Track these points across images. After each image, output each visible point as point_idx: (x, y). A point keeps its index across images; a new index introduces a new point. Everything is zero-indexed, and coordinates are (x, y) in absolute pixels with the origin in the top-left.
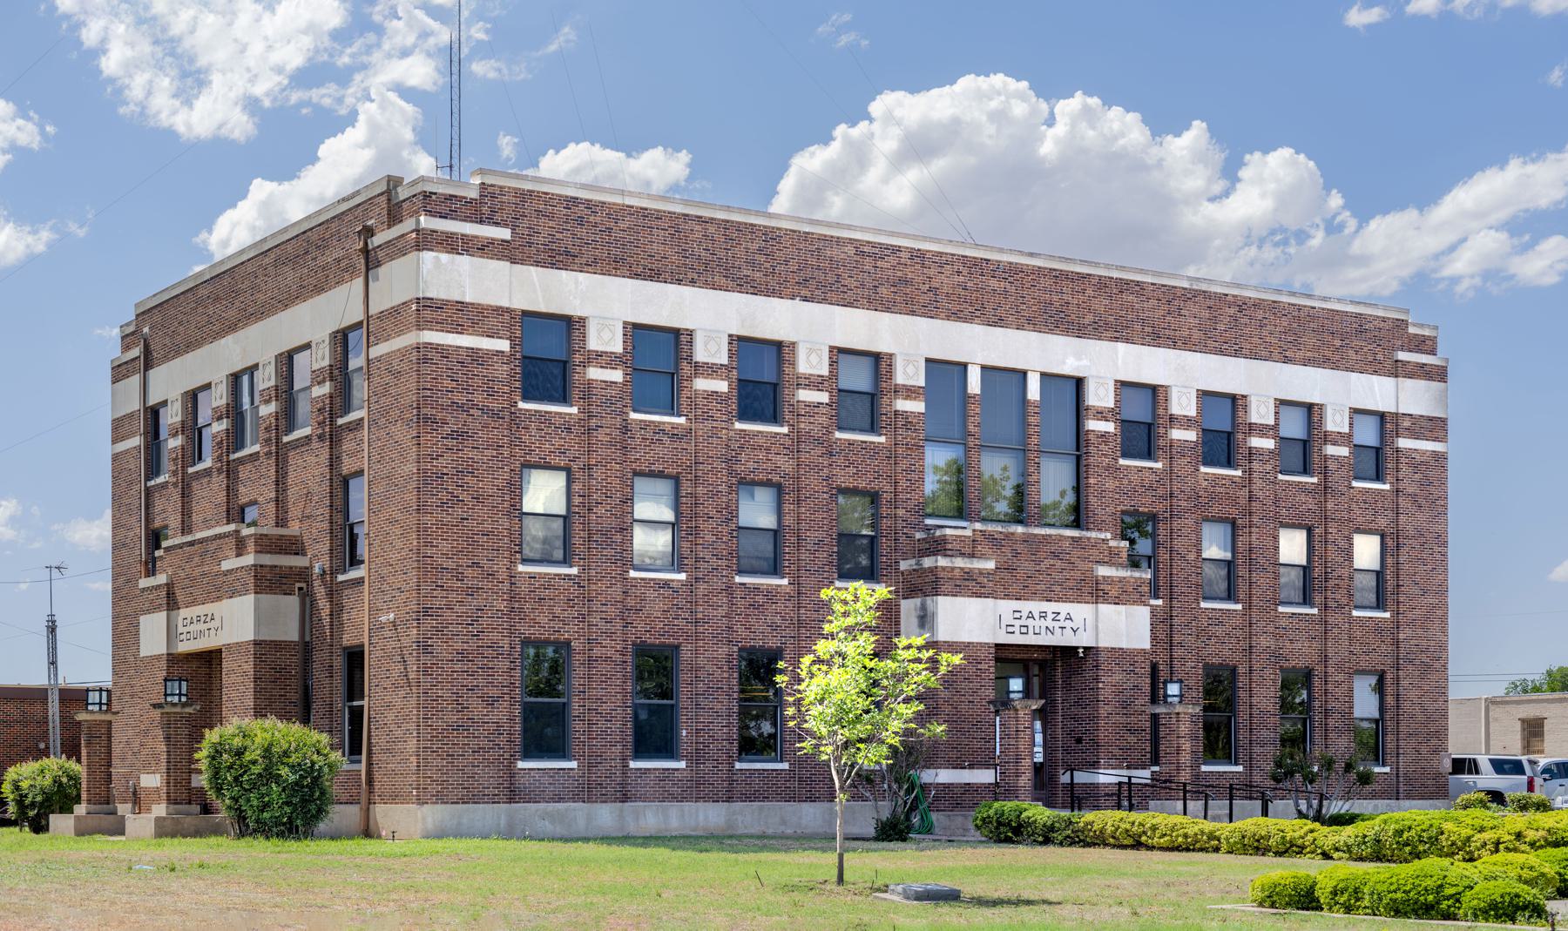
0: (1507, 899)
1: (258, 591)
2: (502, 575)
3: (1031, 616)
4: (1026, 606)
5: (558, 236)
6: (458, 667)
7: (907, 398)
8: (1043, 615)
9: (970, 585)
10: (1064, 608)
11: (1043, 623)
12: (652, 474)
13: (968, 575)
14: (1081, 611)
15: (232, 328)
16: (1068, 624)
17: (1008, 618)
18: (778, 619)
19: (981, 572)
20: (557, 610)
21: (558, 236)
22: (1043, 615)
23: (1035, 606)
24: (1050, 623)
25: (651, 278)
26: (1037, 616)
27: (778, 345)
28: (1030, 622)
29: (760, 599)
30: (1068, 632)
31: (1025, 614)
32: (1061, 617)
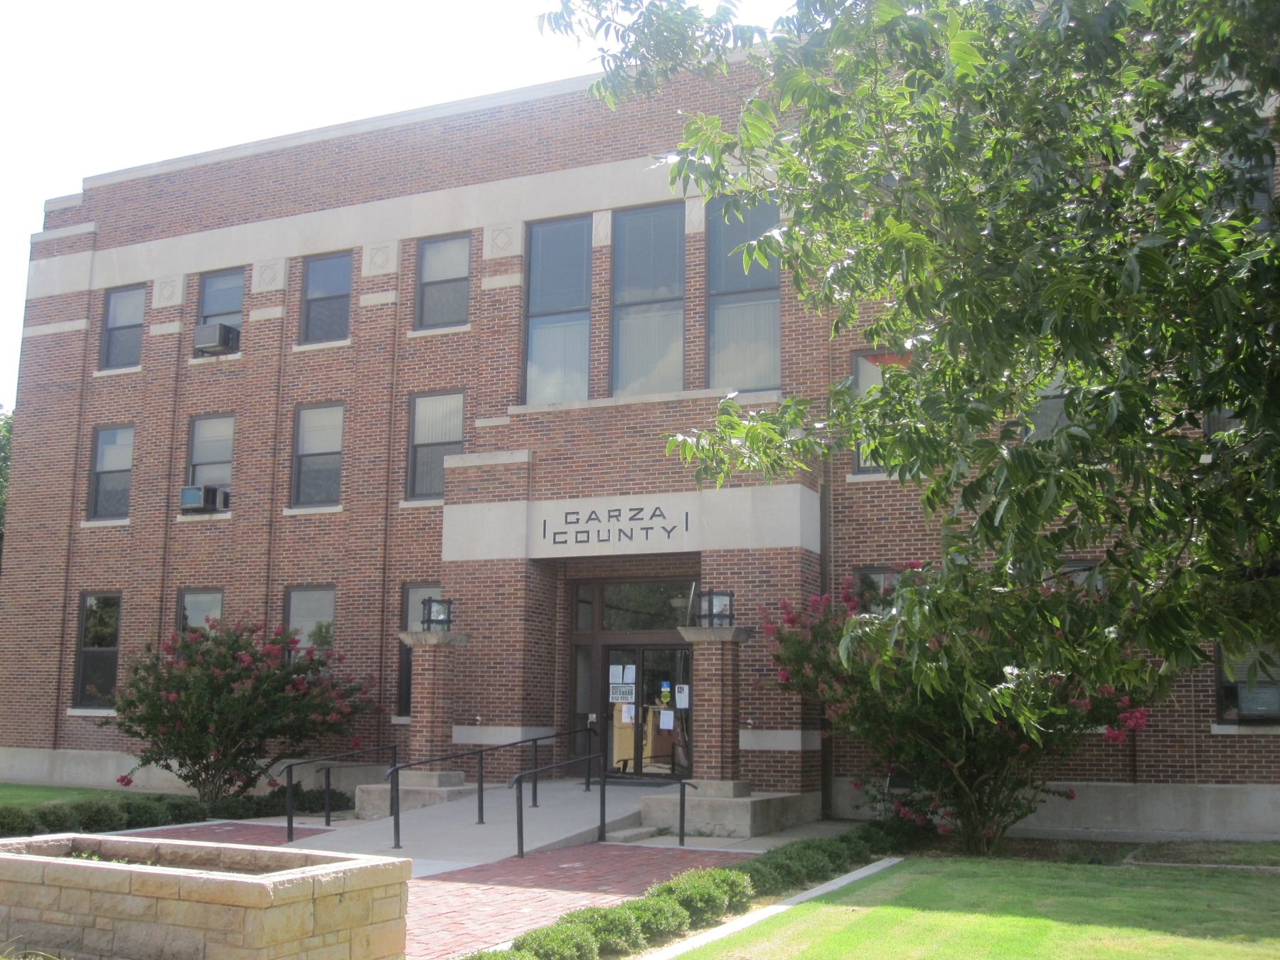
0: (440, 703)
1: (523, 725)
2: (64, 530)
3: (593, 517)
4: (584, 506)
5: (140, 214)
6: (22, 620)
7: (495, 273)
8: (615, 514)
9: (490, 487)
10: (648, 502)
11: (615, 525)
12: (215, 415)
13: (488, 473)
14: (675, 504)
15: (381, 198)
16: (658, 522)
17: (556, 524)
18: (330, 553)
19: (507, 468)
20: (111, 562)
21: (140, 214)
22: (615, 514)
23: (602, 504)
24: (625, 523)
25: (219, 226)
26: (603, 515)
27: (348, 253)
28: (593, 526)
29: (311, 531)
30: (639, 535)
31: (583, 517)
32: (646, 514)
